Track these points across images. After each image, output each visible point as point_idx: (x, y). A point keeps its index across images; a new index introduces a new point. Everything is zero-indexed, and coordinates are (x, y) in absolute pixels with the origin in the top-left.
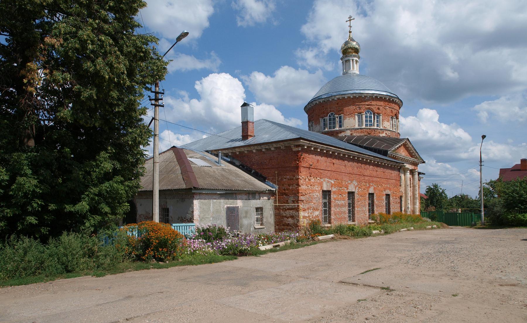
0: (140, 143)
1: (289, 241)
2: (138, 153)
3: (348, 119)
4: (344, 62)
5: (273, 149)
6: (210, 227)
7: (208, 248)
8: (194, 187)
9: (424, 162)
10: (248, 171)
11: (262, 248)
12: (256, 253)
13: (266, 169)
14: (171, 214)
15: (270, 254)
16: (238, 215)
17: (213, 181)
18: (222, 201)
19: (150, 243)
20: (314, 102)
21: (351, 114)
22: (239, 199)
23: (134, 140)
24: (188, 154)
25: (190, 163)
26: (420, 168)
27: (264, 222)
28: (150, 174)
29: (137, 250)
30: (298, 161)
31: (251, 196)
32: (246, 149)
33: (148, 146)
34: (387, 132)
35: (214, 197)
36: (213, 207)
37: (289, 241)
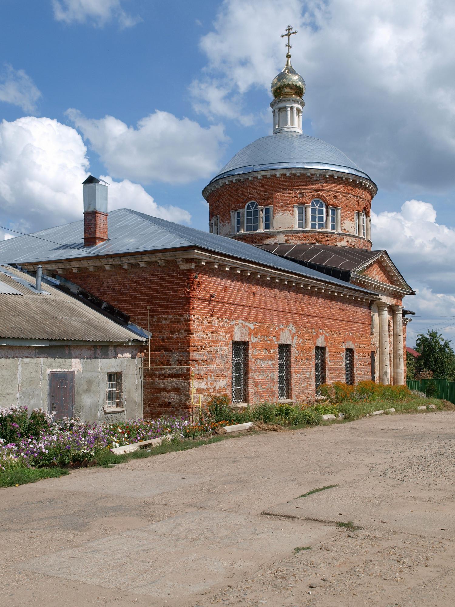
3: (281, 213)
4: (277, 111)
6: (14, 411)
9: (413, 293)
11: (119, 451)
12: (107, 460)
20: (221, 181)
21: (287, 206)
26: (407, 303)
34: (349, 239)
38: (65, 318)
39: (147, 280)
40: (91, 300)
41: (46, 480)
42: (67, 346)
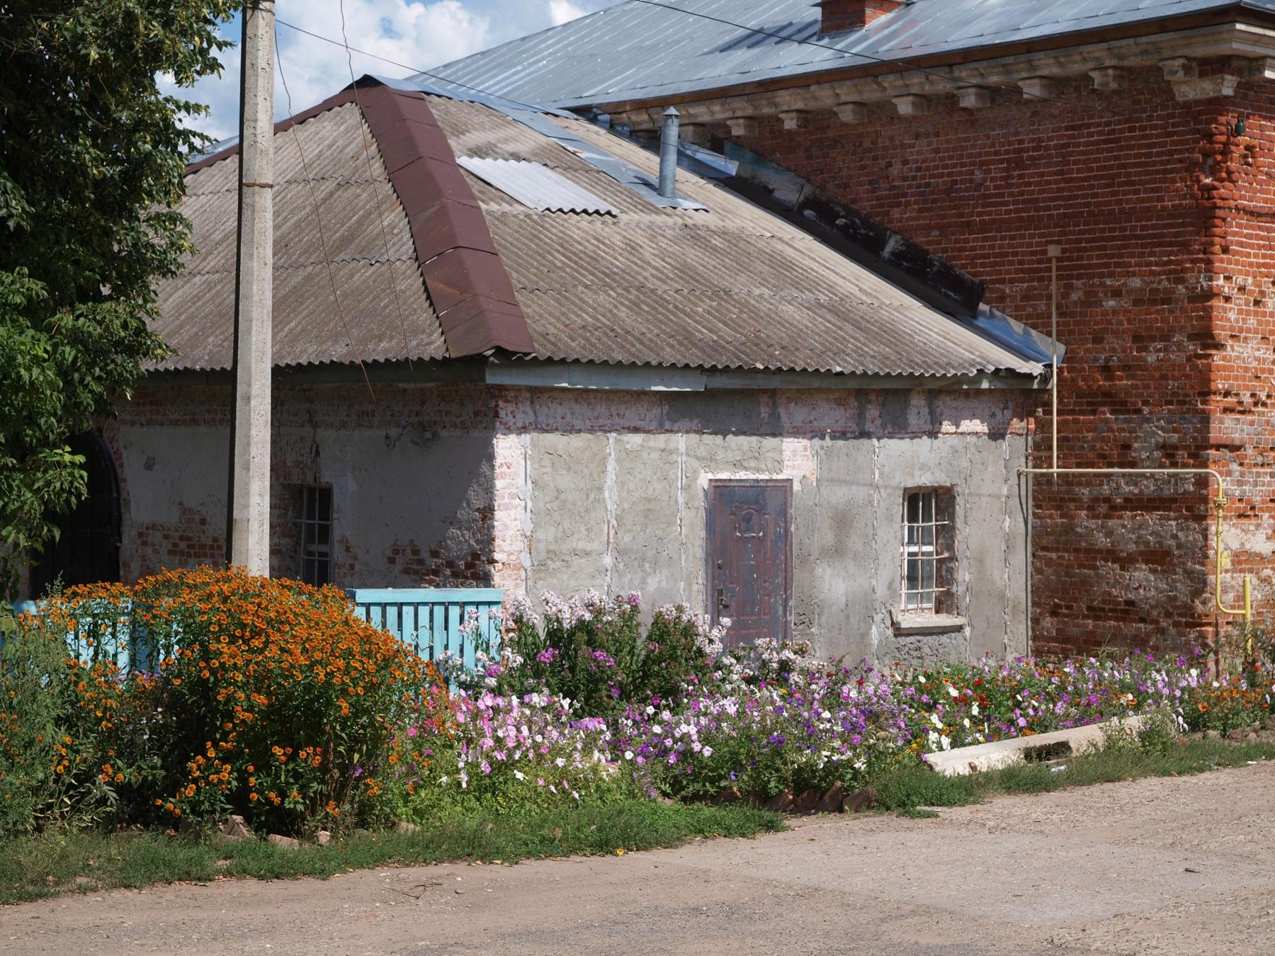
0: (156, 56)
1: (1134, 722)
2: (139, 125)
5: (1033, 90)
6: (598, 612)
7: (593, 755)
8: (500, 352)
10: (859, 242)
11: (950, 762)
12: (908, 792)
13: (984, 227)
14: (341, 527)
15: (1003, 805)
16: (786, 536)
17: (623, 313)
18: (681, 441)
19: (213, 711)
22: (797, 432)
23: (121, 35)
24: (459, 131)
25: (476, 187)
27: (959, 589)
28: (212, 263)
29: (130, 753)
30: (1213, 172)
31: (873, 412)
32: (847, 92)
33: (209, 79)
35: (632, 417)
36: (621, 485)
37: (1134, 722)
38: (757, 292)
39: (1047, 148)
40: (844, 229)
41: (710, 842)
42: (765, 391)
